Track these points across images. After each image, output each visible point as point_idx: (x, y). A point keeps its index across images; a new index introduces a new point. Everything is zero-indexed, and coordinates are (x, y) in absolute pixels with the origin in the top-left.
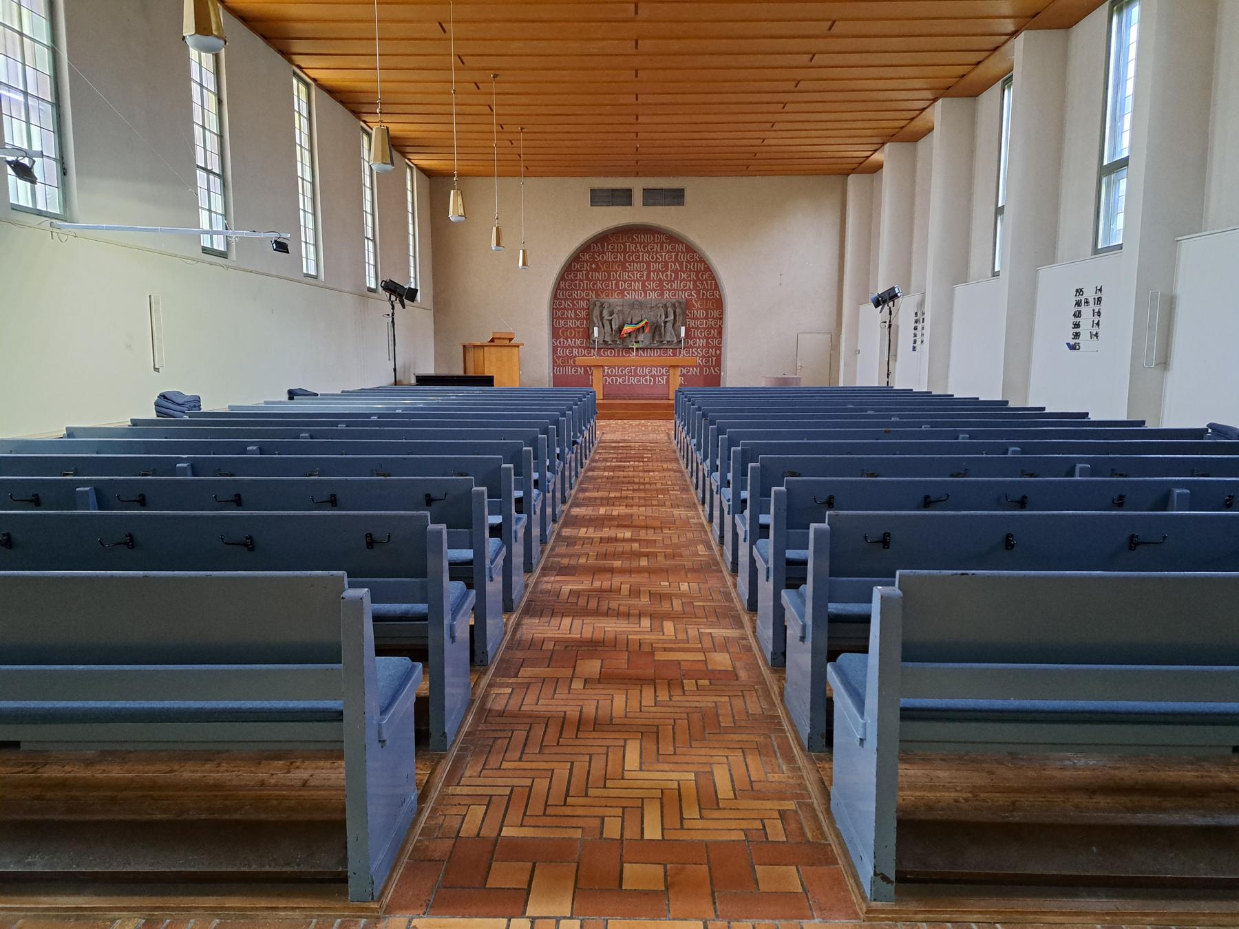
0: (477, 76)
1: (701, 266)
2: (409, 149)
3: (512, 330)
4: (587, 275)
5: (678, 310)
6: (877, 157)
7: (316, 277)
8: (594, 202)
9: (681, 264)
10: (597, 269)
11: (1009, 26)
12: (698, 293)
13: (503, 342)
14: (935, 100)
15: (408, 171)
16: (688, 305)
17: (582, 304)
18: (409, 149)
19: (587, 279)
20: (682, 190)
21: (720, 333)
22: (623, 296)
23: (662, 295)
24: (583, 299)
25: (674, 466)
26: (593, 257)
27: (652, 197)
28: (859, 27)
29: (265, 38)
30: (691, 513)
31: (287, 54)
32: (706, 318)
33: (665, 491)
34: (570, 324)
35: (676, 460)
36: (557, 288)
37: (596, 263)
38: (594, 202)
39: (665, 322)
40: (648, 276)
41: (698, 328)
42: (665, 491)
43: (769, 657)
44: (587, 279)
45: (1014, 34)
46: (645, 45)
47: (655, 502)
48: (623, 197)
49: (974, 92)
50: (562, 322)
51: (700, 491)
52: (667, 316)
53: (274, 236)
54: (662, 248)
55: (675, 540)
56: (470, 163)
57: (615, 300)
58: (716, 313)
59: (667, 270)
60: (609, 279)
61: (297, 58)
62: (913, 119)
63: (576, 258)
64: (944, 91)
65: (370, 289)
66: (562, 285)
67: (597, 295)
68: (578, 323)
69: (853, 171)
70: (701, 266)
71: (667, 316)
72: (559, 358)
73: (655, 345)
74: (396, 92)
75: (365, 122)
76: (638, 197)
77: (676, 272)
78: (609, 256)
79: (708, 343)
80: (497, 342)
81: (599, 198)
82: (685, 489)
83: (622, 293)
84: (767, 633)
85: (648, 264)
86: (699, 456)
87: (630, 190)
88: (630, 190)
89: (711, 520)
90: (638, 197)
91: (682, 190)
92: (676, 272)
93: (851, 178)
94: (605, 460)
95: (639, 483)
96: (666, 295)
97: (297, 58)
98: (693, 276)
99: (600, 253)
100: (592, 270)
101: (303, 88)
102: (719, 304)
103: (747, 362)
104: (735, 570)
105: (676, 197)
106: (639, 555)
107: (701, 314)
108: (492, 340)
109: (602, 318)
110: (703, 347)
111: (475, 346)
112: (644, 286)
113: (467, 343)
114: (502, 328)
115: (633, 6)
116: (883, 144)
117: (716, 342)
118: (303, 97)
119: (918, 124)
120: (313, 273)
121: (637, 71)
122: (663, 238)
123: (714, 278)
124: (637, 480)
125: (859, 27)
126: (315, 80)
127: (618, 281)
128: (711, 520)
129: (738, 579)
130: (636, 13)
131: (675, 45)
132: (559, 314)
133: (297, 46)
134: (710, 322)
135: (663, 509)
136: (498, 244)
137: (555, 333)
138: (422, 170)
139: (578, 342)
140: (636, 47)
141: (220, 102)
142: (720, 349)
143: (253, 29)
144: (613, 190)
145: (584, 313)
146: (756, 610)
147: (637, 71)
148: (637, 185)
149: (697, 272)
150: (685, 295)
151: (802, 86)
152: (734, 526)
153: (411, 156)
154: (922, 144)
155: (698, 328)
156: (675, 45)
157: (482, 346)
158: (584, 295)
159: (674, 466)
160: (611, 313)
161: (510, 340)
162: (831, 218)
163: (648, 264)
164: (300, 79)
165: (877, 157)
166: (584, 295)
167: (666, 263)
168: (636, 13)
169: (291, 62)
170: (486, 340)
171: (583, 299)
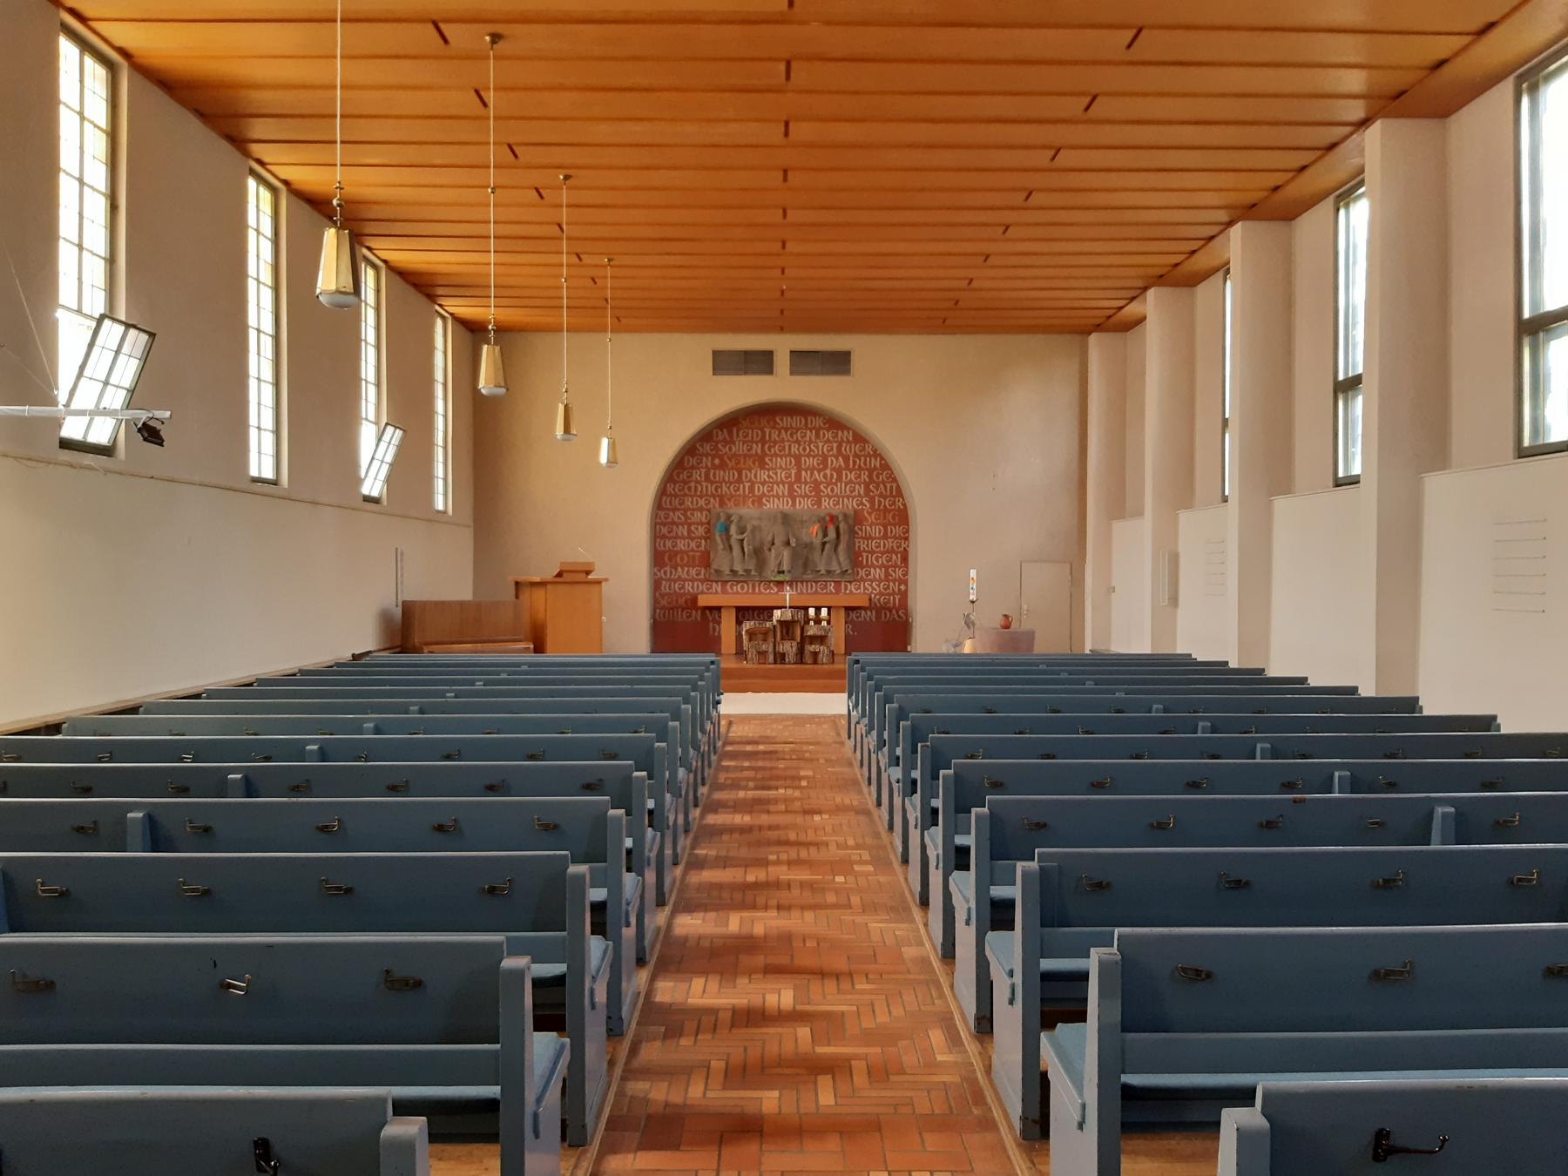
0: (537, 178)
1: (875, 463)
2: (440, 291)
3: (590, 559)
4: (707, 475)
5: (842, 526)
6: (1133, 309)
7: (275, 483)
8: (717, 370)
9: (846, 459)
10: (723, 466)
11: (1357, 111)
12: (872, 501)
13: (576, 577)
14: (1230, 224)
15: (439, 322)
16: (857, 519)
17: (699, 516)
18: (440, 291)
19: (707, 479)
20: (848, 354)
21: (905, 559)
22: (761, 504)
23: (819, 503)
24: (701, 509)
25: (850, 799)
26: (716, 448)
27: (803, 362)
28: (1138, 108)
29: (202, 115)
30: (901, 930)
31: (240, 143)
32: (885, 537)
33: (844, 866)
34: (681, 545)
35: (850, 764)
36: (662, 492)
37: (721, 458)
38: (717, 370)
39: (824, 544)
40: (798, 476)
41: (872, 552)
42: (844, 866)
43: (1017, 1125)
44: (707, 479)
45: (1364, 123)
46: (800, 131)
47: (831, 898)
48: (760, 362)
49: (1289, 213)
50: (669, 544)
51: (874, 788)
52: (825, 535)
53: (143, 416)
54: (817, 436)
55: (882, 1018)
56: (538, 311)
57: (748, 511)
58: (899, 530)
59: (826, 467)
60: (740, 480)
61: (256, 149)
62: (1194, 252)
63: (690, 451)
64: (1249, 211)
65: (368, 499)
66: (670, 489)
67: (722, 504)
68: (693, 545)
69: (1098, 328)
70: (875, 463)
71: (825, 535)
72: (663, 596)
73: (809, 576)
74: (408, 204)
75: (369, 249)
76: (782, 362)
77: (839, 471)
78: (739, 448)
79: (887, 574)
80: (566, 577)
81: (725, 363)
82: (881, 863)
83: (759, 501)
84: (886, 817)
85: (798, 458)
86: (862, 728)
87: (771, 353)
88: (771, 353)
89: (879, 804)
90: (782, 362)
91: (848, 354)
92: (839, 471)
93: (1093, 339)
94: (735, 785)
95: (798, 844)
96: (825, 503)
97: (256, 149)
98: (865, 476)
99: (726, 443)
100: (715, 467)
101: (266, 195)
102: (903, 517)
103: (952, 606)
104: (905, 860)
105: (839, 363)
106: (816, 1068)
107: (876, 531)
108: (559, 575)
109: (728, 537)
110: (880, 581)
111: (533, 584)
112: (791, 490)
113: (521, 578)
114: (579, 554)
115: (782, 67)
116: (1145, 289)
117: (899, 573)
118: (266, 207)
119: (1202, 261)
120: (268, 474)
121: (785, 171)
122: (819, 422)
123: (895, 480)
124: (792, 836)
125: (1138, 108)
126: (286, 183)
127: (753, 484)
128: (879, 804)
129: (930, 915)
130: (788, 77)
131: (847, 132)
132: (665, 530)
133: (258, 128)
134: (890, 543)
135: (847, 917)
136: (567, 430)
137: (659, 558)
138: (458, 320)
139: (693, 572)
140: (786, 134)
141: (113, 207)
142: (906, 583)
143: (182, 102)
144: (746, 352)
145: (701, 531)
146: (954, 957)
147: (785, 171)
148: (782, 345)
149: (871, 472)
150: (851, 505)
151: (1036, 199)
152: (923, 847)
153: (443, 301)
154: (1202, 290)
155: (872, 552)
156: (847, 132)
157: (542, 584)
158: (702, 502)
159: (850, 799)
160: (742, 531)
161: (588, 573)
162: (1065, 395)
163: (798, 458)
164: (261, 180)
165: (1133, 309)
166: (702, 502)
167: (825, 458)
168: (788, 77)
169: (247, 154)
170: (549, 573)
171: (701, 509)
